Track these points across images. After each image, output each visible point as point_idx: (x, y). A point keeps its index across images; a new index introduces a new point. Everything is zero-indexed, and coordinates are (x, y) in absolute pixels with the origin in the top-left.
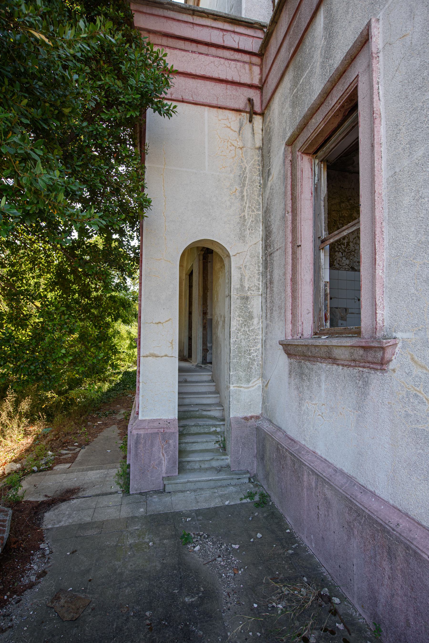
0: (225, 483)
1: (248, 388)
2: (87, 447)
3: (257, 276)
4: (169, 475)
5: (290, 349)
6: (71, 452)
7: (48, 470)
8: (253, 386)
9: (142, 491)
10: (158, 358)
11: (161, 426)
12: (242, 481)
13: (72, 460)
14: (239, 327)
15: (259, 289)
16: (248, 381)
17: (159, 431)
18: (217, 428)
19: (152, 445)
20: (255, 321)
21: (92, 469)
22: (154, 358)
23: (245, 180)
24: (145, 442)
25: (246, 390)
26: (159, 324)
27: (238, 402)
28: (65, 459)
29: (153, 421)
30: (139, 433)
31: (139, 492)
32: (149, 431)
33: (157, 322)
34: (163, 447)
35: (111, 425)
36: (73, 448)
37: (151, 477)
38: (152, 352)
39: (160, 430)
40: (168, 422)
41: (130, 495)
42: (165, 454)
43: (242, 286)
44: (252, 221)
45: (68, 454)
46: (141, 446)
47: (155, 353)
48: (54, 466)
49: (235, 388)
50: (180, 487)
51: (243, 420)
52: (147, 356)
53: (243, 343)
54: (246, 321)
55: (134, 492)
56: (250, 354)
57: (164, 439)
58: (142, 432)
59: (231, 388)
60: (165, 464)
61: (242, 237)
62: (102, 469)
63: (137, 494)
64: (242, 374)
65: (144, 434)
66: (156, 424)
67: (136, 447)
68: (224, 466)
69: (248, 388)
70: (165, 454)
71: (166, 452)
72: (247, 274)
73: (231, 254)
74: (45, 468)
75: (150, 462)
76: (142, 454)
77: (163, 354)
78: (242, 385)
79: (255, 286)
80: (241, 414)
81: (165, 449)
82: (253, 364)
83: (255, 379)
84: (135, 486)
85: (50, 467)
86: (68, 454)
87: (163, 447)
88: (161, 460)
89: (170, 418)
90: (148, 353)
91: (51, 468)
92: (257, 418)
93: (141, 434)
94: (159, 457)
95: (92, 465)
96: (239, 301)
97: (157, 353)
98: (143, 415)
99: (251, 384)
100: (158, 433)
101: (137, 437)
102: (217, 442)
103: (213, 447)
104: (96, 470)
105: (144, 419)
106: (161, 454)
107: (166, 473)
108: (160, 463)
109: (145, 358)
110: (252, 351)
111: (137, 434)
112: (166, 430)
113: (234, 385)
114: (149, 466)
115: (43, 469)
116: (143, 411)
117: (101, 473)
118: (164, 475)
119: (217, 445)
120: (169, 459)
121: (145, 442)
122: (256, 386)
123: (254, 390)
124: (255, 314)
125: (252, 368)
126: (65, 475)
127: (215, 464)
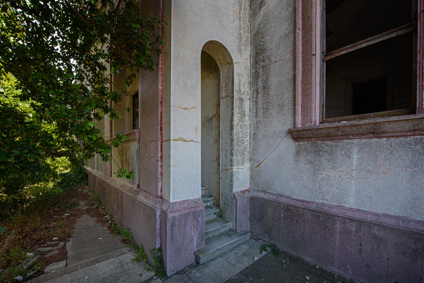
0: (237, 243)
1: (243, 169)
2: (71, 239)
3: (247, 85)
4: (199, 249)
5: (296, 135)
6: (55, 248)
7: (39, 275)
8: (245, 168)
9: (178, 270)
10: (185, 143)
11: (191, 206)
12: (246, 239)
13: (63, 255)
14: (238, 122)
15: (248, 94)
16: (243, 164)
17: (190, 211)
18: (207, 203)
19: (185, 225)
20: (247, 118)
21: (98, 261)
22: (183, 142)
23: (241, 5)
24: (180, 224)
25: (242, 171)
26: (186, 110)
27: (238, 180)
28: (52, 257)
29: (183, 202)
30: (174, 215)
31: (175, 272)
32: (183, 212)
33: (185, 107)
34: (193, 225)
35: (81, 215)
36: (53, 243)
37: (185, 255)
38: (180, 136)
39: (191, 209)
40: (195, 201)
41: (168, 278)
42: (195, 231)
43: (240, 89)
44: (245, 40)
45: (53, 250)
46: (176, 228)
47: (183, 137)
48: (44, 268)
49: (236, 169)
50: (211, 257)
51: (241, 194)
52: (176, 140)
53: (240, 135)
54: (242, 117)
55: (171, 274)
56: (244, 143)
57: (194, 218)
58: (176, 214)
59: (234, 169)
60: (195, 239)
61: (240, 50)
62: (109, 258)
63: (174, 275)
64: (240, 158)
65: (178, 216)
66: (186, 205)
67: (172, 230)
68: (228, 231)
69: (243, 169)
70: (195, 231)
71: (196, 229)
72: (242, 80)
73: (234, 61)
74: (35, 274)
75: (184, 241)
76: (177, 235)
77: (190, 139)
78: (240, 167)
79: (246, 91)
80: (239, 190)
81: (196, 226)
82: (245, 151)
83: (246, 162)
84: (172, 267)
85: (39, 271)
86: (53, 250)
87: (193, 225)
88: (193, 237)
89: (195, 198)
90: (177, 137)
91: (41, 272)
92: (248, 191)
93: (176, 217)
94: (191, 235)
95: (93, 257)
96: (238, 100)
97: (184, 137)
98: (174, 198)
99: (244, 167)
100: (190, 213)
101: (173, 220)
102: (215, 213)
103: (213, 218)
104: (104, 260)
105: (175, 201)
106: (193, 232)
107: (197, 248)
108: (192, 240)
109: (175, 142)
110: (245, 141)
111: (173, 217)
112: (197, 209)
113: (236, 167)
114: (184, 245)
115: (31, 276)
116: (173, 194)
117: (113, 262)
118: (195, 250)
119: (215, 216)
120: (199, 234)
121: (180, 224)
122: (247, 168)
123: (246, 171)
124: (246, 114)
125: (244, 154)
126: (68, 275)
127: (222, 231)
